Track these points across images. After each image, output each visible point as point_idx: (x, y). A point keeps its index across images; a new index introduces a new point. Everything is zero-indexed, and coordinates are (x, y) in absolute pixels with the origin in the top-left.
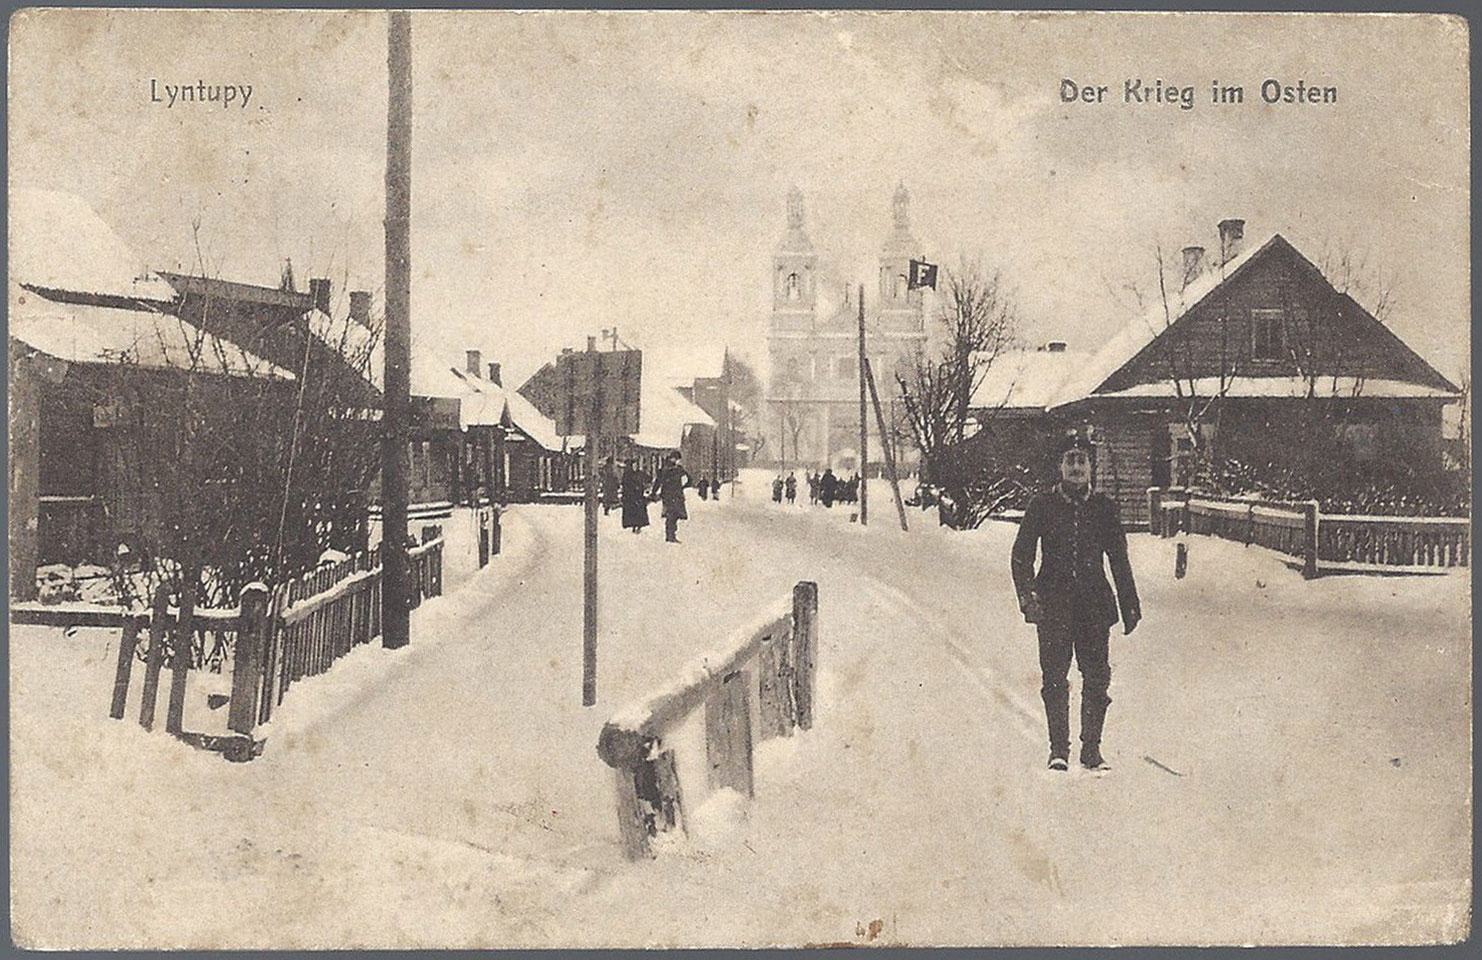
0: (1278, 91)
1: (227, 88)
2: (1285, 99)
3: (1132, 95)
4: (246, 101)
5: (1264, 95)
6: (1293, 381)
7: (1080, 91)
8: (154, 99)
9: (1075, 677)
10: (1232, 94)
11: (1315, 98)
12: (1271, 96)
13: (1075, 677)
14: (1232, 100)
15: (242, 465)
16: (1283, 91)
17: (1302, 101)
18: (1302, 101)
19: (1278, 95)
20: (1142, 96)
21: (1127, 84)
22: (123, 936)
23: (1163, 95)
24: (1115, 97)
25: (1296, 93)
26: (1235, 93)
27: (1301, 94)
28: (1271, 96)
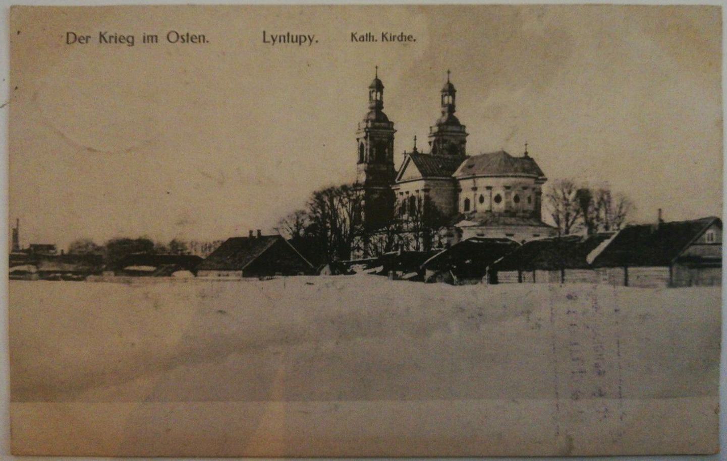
3: (384, 39)
17: (152, 42)
18: (292, 41)
20: (108, 39)
24: (138, 39)
26: (153, 39)
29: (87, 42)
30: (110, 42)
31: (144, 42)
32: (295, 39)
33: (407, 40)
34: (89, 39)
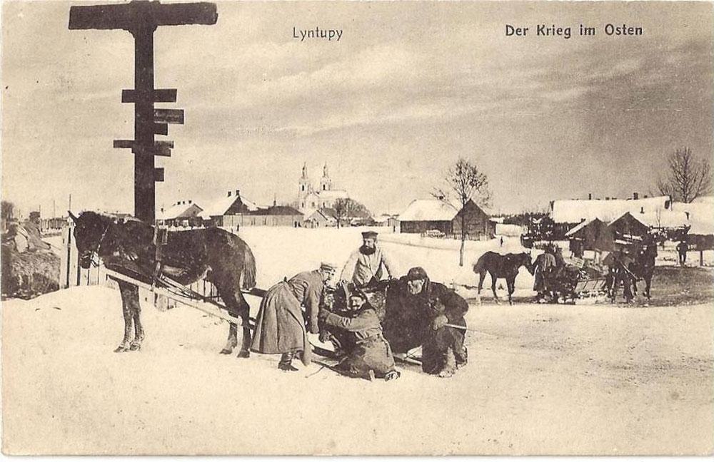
0: (613, 31)
1: (330, 31)
2: (617, 34)
4: (340, 36)
5: (606, 31)
6: (119, 144)
7: (515, 29)
8: (294, 37)
9: (682, 256)
10: (590, 32)
11: (519, 33)
12: (610, 32)
13: (682, 256)
14: (590, 34)
15: (623, 235)
16: (615, 30)
19: (613, 31)
21: (538, 26)
22: (523, 358)
23: (556, 33)
25: (622, 31)
27: (624, 31)
28: (610, 32)
29: (525, 34)
30: (548, 34)
31: (581, 34)
32: (324, 34)
33: (556, 33)
34: (526, 31)
